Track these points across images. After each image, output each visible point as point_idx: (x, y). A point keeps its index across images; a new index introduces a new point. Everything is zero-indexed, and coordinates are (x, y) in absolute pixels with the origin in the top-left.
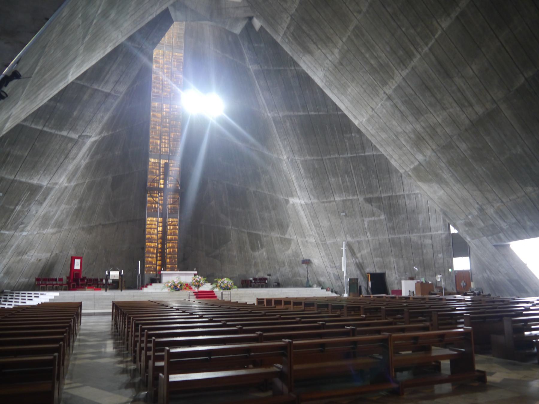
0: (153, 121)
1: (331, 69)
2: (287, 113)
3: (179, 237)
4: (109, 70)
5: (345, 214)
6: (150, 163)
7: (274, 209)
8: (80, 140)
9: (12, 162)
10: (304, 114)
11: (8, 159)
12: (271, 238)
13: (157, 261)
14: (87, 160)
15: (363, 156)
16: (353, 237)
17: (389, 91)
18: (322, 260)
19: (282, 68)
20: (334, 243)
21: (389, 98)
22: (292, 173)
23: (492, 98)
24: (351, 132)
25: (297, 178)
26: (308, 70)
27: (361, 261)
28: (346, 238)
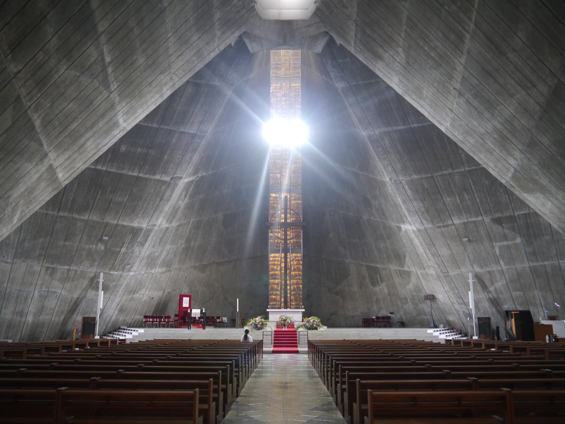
2: (384, 129)
3: (303, 273)
4: (193, 112)
5: (468, 239)
6: (271, 199)
7: (388, 238)
8: (173, 182)
9: (115, 208)
10: (405, 127)
11: (111, 205)
12: (390, 271)
13: (281, 297)
14: (186, 200)
16: (482, 267)
17: (458, 86)
18: (447, 296)
20: (458, 274)
21: (460, 94)
22: (398, 196)
23: (551, 71)
25: (404, 202)
26: (384, 78)
27: (495, 296)
28: (473, 268)
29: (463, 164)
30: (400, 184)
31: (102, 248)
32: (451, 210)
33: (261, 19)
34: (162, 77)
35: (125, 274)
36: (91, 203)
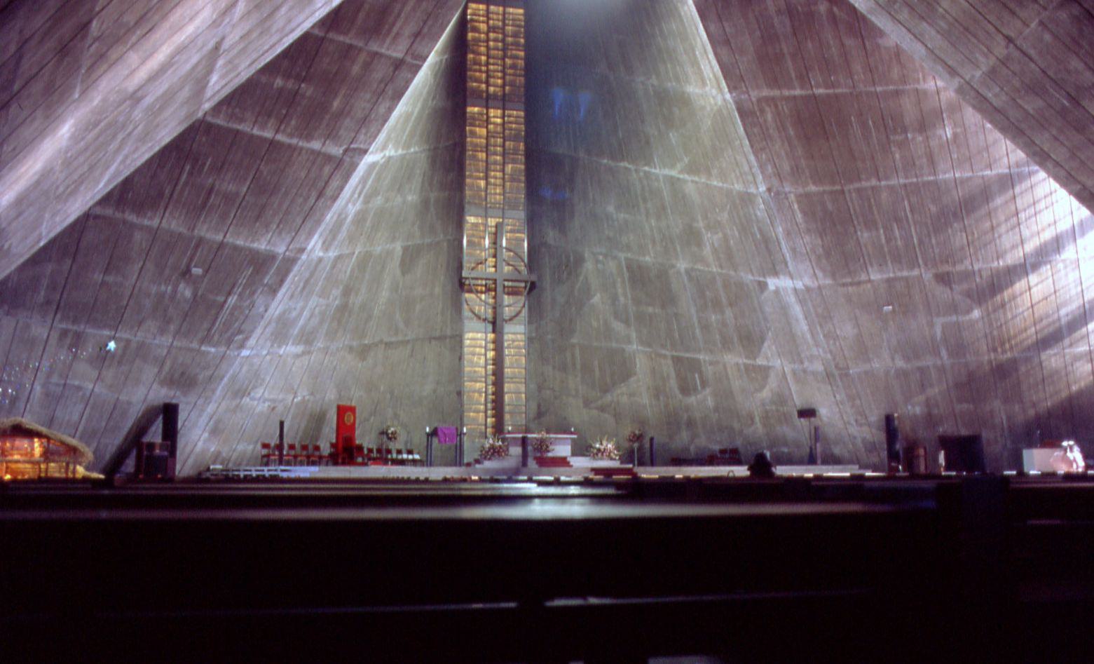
0: (471, 143)
7: (731, 305)
8: (347, 159)
10: (803, 93)
11: (211, 200)
12: (725, 366)
13: (486, 417)
20: (866, 373)
24: (905, 131)
25: (788, 234)
29: (897, 172)
31: (188, 293)
32: (869, 255)
35: (232, 353)
36: (167, 192)
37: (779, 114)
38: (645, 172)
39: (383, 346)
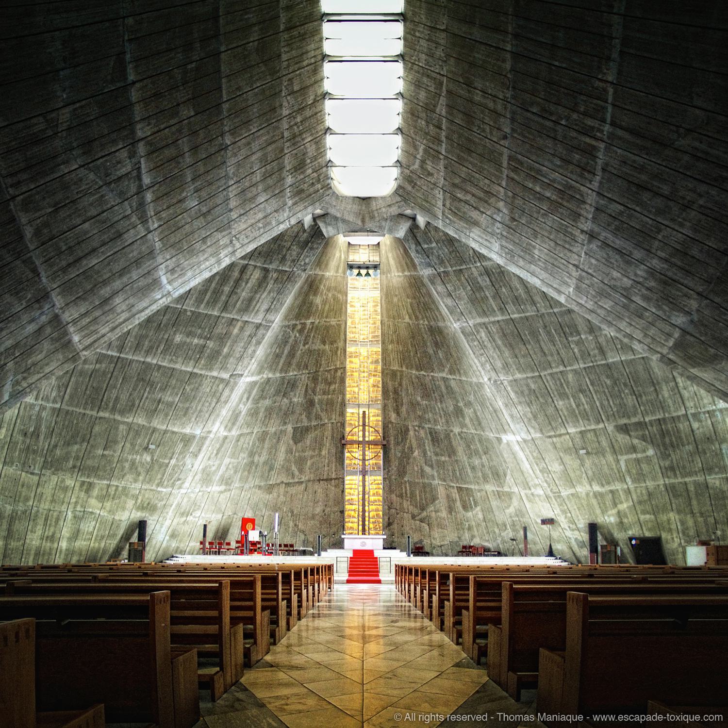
1: (505, 233)
3: (383, 499)
6: (348, 415)
8: (232, 380)
14: (249, 405)
15: (604, 364)
17: (587, 226)
19: (464, 267)
30: (502, 386)
31: (149, 459)
32: (565, 417)
33: (337, 197)
34: (219, 235)
35: (175, 491)
37: (489, 332)
38: (432, 376)
39: (284, 485)
